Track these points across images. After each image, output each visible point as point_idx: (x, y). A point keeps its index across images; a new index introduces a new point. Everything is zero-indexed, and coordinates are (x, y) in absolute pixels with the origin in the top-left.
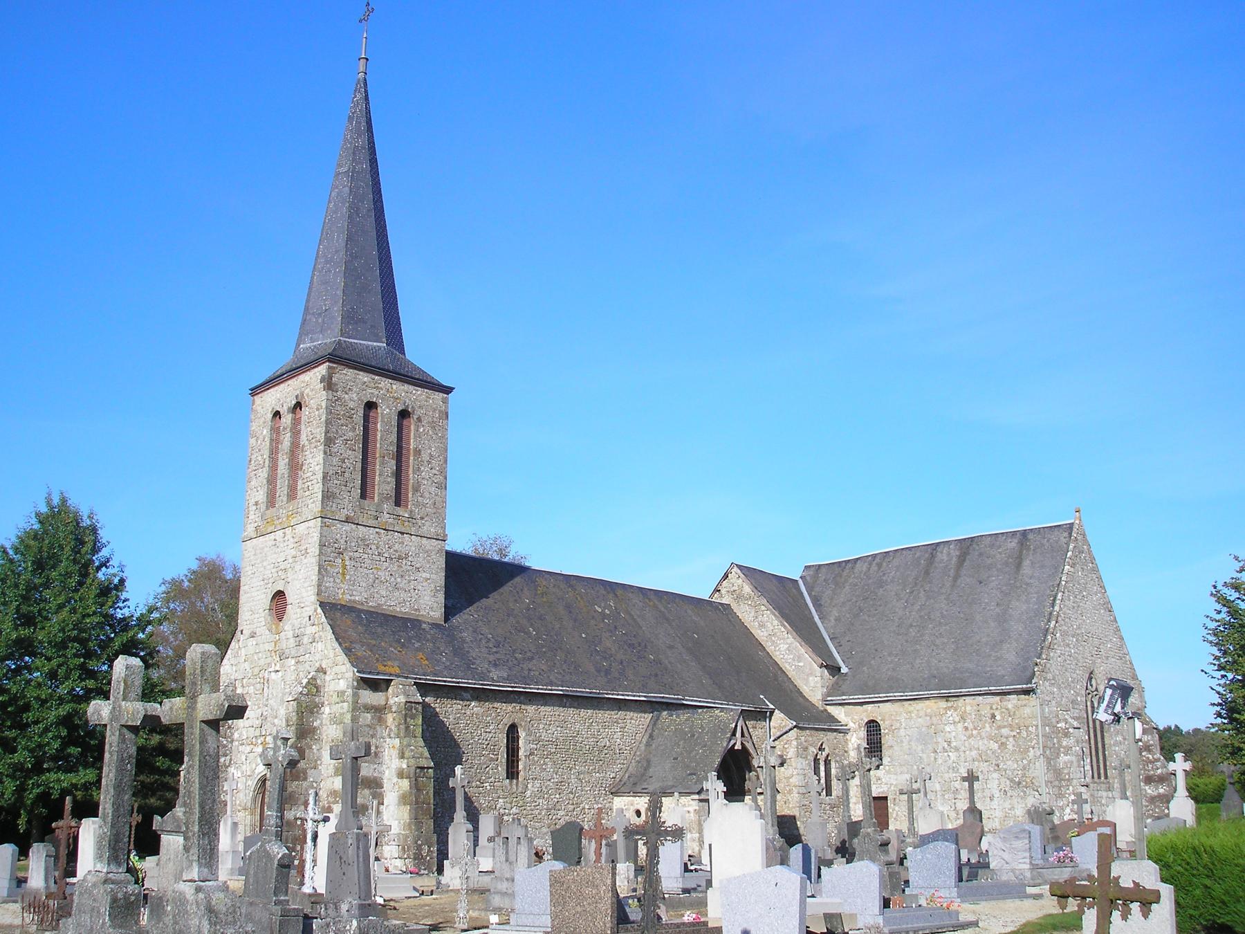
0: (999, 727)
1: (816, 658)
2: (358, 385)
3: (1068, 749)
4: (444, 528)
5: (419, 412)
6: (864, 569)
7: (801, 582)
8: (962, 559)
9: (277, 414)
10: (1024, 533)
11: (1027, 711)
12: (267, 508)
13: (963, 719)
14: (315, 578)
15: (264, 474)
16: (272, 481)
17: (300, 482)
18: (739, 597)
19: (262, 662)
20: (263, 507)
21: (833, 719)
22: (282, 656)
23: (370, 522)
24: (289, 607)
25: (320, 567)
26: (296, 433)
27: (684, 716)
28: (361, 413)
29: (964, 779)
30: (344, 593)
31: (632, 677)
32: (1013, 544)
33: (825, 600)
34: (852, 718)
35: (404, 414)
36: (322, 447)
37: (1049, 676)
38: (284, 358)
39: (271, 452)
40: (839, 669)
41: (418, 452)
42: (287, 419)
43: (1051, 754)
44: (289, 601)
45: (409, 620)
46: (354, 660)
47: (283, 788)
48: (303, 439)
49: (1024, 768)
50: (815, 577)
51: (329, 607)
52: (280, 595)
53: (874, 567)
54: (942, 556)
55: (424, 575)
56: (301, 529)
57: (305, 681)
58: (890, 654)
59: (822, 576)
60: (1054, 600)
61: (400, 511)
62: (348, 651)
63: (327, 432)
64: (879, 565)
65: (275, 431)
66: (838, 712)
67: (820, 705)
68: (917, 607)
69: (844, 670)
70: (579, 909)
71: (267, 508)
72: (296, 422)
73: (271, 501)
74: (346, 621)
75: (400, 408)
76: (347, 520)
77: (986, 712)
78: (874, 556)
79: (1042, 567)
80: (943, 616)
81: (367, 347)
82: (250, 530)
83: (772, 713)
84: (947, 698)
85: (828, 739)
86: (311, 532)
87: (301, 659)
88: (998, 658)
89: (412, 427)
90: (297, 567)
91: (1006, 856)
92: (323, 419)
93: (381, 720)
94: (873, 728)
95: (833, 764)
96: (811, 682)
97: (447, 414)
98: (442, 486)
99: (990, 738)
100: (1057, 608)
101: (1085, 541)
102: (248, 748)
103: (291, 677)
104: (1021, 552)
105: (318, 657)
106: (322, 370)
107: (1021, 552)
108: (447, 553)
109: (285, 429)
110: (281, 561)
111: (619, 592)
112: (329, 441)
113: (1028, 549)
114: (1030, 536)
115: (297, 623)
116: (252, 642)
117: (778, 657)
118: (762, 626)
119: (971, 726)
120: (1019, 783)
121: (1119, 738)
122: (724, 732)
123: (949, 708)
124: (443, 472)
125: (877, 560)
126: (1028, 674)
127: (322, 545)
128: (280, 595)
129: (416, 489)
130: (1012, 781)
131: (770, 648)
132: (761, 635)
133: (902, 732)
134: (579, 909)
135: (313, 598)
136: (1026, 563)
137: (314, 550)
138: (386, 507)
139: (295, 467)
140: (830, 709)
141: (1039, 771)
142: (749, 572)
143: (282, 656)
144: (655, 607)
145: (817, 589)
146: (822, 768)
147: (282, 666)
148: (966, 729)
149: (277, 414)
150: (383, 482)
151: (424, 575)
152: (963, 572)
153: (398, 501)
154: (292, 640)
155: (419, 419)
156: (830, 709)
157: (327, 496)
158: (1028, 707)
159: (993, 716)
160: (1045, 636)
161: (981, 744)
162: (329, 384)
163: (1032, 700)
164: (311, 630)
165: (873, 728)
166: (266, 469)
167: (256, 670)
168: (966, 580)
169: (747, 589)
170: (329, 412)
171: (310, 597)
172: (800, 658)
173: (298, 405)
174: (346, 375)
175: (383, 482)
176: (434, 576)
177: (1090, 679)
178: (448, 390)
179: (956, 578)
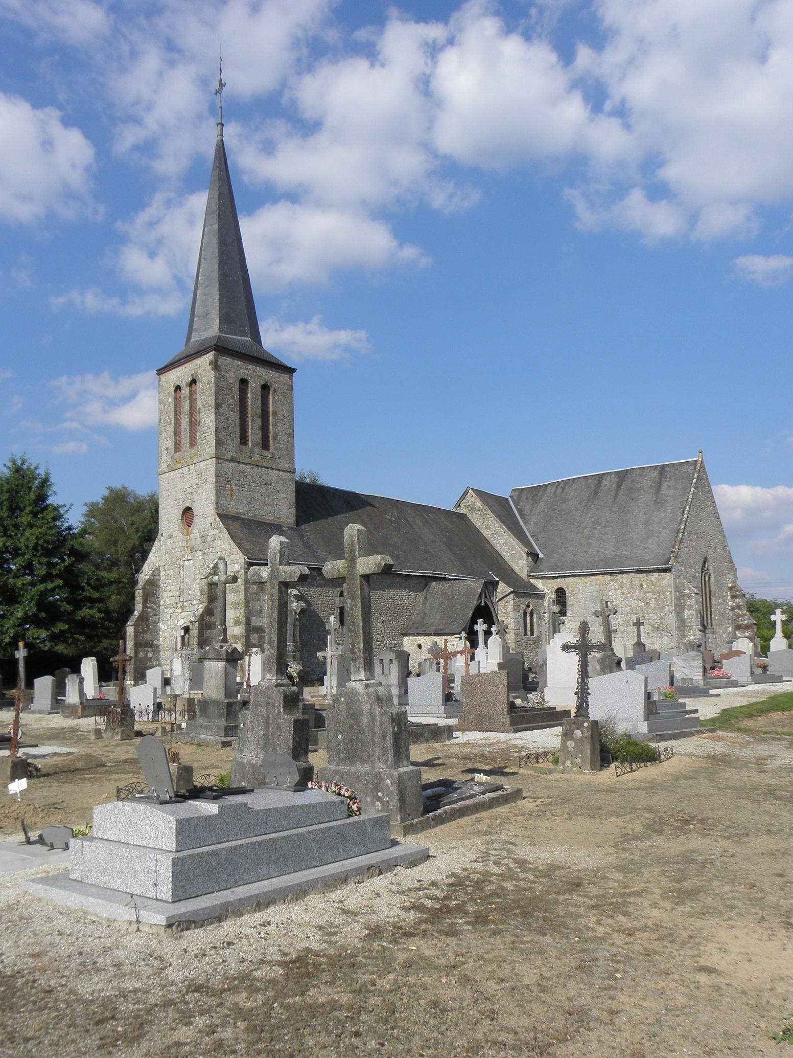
0: (645, 593)
1: (524, 548)
2: (236, 368)
3: (690, 607)
4: (293, 464)
5: (274, 386)
6: (553, 491)
7: (510, 500)
8: (619, 486)
9: (178, 388)
10: (663, 467)
11: (665, 582)
12: (176, 452)
13: (621, 587)
14: (213, 498)
15: (171, 429)
16: (177, 433)
17: (198, 434)
18: (472, 509)
19: (178, 554)
20: (172, 451)
21: (534, 587)
22: (193, 550)
23: (247, 461)
24: (195, 518)
25: (217, 491)
26: (193, 400)
27: (447, 585)
28: (237, 386)
29: (634, 624)
30: (233, 508)
31: (412, 560)
32: (655, 474)
33: (527, 511)
34: (547, 588)
35: (265, 388)
36: (213, 410)
37: (680, 560)
38: (178, 348)
39: (175, 414)
40: (538, 555)
41: (275, 413)
42: (186, 391)
43: (679, 608)
44: (195, 513)
45: (274, 525)
46: (245, 552)
47: (201, 635)
48: (199, 404)
49: (662, 619)
50: (519, 497)
51: (224, 517)
52: (188, 510)
53: (560, 490)
54: (606, 482)
55: (283, 495)
56: (201, 465)
57: (211, 566)
58: (572, 546)
59: (524, 496)
60: (684, 511)
61: (265, 453)
62: (240, 546)
63: (216, 399)
64: (563, 489)
65: (177, 399)
66: (539, 584)
67: (525, 577)
68: (589, 515)
69: (541, 556)
70: (483, 700)
71: (176, 452)
72: (192, 393)
73: (178, 447)
74: (237, 526)
75: (263, 382)
76: (232, 460)
77: (636, 583)
78: (559, 483)
79: (676, 489)
80: (607, 522)
81: (238, 340)
82: (164, 467)
83: (497, 583)
84: (611, 574)
85: (533, 602)
86: (209, 467)
87: (206, 551)
88: (645, 548)
89: (271, 396)
90: (200, 492)
91: (686, 671)
92: (213, 390)
93: (263, 590)
94: (560, 592)
95: (535, 616)
96: (520, 565)
97: (292, 387)
98: (291, 436)
99: (639, 599)
100: (685, 516)
101: (705, 473)
102: (171, 611)
103: (199, 563)
104: (660, 480)
105: (218, 549)
106: (210, 356)
107: (660, 480)
108: (297, 482)
109: (185, 398)
110: (186, 487)
111: (400, 506)
112: (218, 406)
113: (666, 477)
114: (667, 469)
115: (201, 528)
116: (170, 541)
117: (498, 548)
118: (488, 528)
119: (626, 592)
120: (658, 628)
121: (720, 601)
122: (474, 595)
123: (612, 580)
124: (291, 427)
125: (562, 485)
126: (666, 558)
127: (217, 476)
128: (188, 510)
129: (275, 438)
130: (653, 626)
131: (493, 541)
132: (486, 533)
133: (580, 596)
134: (483, 700)
135: (213, 511)
136: (664, 487)
137: (212, 479)
138: (257, 450)
139: (194, 424)
140: (532, 581)
141: (672, 620)
142: (480, 494)
143: (193, 550)
144: (422, 516)
145: (521, 504)
146: (528, 618)
147: (193, 556)
148: (623, 593)
149: (178, 388)
150: (254, 434)
151: (283, 495)
152: (621, 492)
153: (265, 445)
154: (199, 539)
155: (275, 391)
156: (532, 581)
157: (219, 443)
158: (667, 580)
159: (642, 585)
160: (678, 534)
161: (634, 603)
162: (216, 366)
163: (669, 576)
164: (212, 532)
165: (560, 592)
166: (172, 426)
167: (174, 560)
168: (622, 497)
169: (478, 504)
170: (217, 386)
171: (210, 510)
172: (513, 548)
173: (194, 382)
174: (226, 361)
175: (254, 434)
176: (288, 496)
177: (704, 563)
178: (291, 371)
179: (616, 495)
